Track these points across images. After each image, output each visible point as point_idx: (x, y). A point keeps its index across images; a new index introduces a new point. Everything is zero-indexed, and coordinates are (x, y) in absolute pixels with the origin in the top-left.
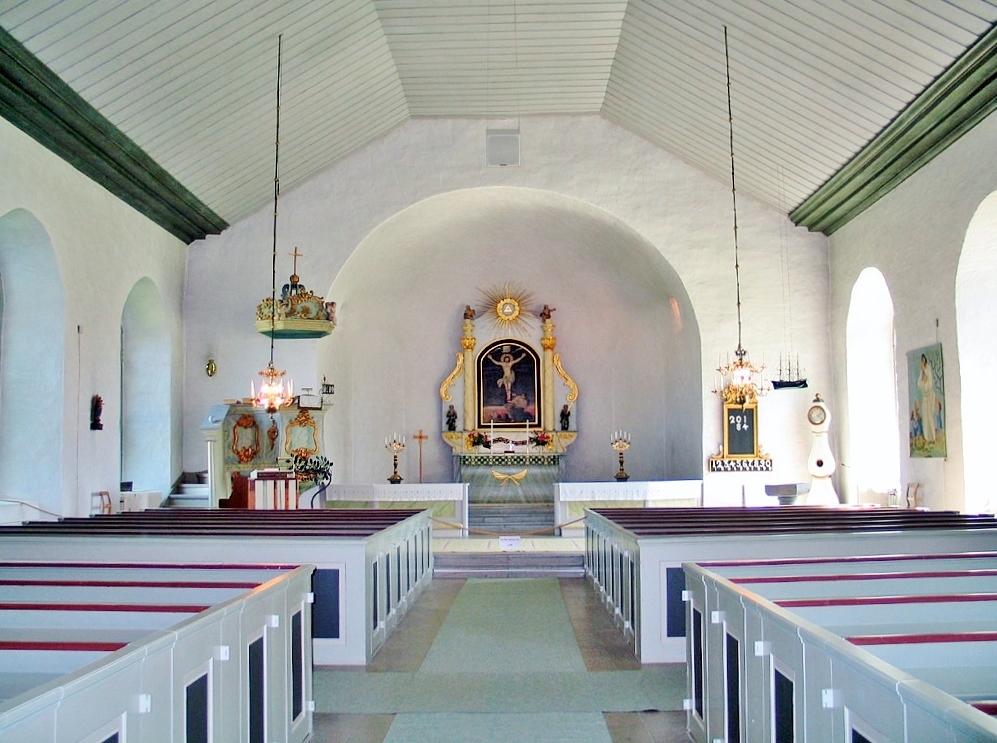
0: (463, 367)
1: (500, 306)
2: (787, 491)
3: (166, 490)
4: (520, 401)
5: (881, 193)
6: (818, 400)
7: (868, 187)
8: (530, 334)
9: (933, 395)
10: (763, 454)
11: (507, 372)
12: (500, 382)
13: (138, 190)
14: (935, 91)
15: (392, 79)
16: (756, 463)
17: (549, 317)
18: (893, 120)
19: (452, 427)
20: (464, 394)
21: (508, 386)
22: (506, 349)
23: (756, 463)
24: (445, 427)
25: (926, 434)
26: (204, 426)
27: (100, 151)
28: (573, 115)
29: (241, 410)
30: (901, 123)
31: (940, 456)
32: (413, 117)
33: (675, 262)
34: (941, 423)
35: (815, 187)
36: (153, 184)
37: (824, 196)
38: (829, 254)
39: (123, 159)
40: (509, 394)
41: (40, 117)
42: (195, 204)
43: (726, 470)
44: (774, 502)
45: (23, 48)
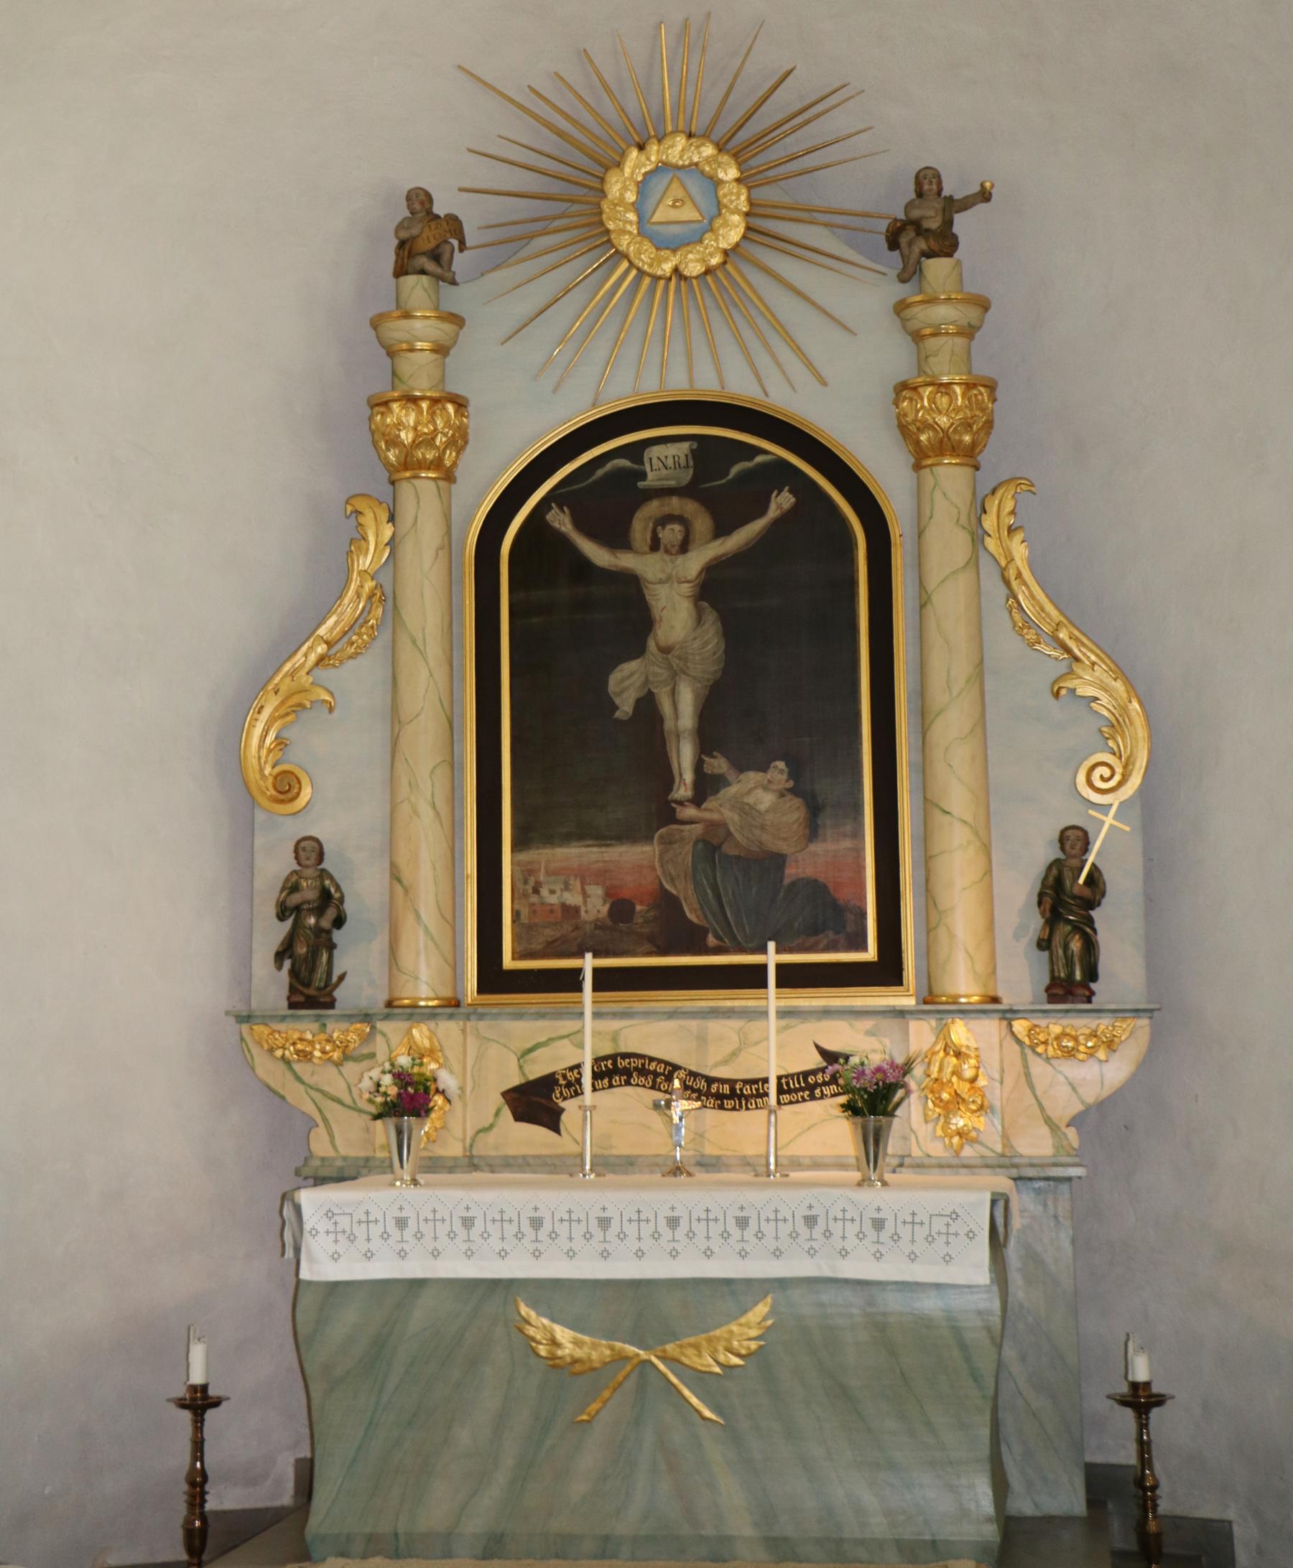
4: (758, 800)
8: (830, 366)
11: (675, 613)
12: (625, 683)
20: (398, 792)
21: (682, 710)
22: (667, 458)
40: (684, 756)
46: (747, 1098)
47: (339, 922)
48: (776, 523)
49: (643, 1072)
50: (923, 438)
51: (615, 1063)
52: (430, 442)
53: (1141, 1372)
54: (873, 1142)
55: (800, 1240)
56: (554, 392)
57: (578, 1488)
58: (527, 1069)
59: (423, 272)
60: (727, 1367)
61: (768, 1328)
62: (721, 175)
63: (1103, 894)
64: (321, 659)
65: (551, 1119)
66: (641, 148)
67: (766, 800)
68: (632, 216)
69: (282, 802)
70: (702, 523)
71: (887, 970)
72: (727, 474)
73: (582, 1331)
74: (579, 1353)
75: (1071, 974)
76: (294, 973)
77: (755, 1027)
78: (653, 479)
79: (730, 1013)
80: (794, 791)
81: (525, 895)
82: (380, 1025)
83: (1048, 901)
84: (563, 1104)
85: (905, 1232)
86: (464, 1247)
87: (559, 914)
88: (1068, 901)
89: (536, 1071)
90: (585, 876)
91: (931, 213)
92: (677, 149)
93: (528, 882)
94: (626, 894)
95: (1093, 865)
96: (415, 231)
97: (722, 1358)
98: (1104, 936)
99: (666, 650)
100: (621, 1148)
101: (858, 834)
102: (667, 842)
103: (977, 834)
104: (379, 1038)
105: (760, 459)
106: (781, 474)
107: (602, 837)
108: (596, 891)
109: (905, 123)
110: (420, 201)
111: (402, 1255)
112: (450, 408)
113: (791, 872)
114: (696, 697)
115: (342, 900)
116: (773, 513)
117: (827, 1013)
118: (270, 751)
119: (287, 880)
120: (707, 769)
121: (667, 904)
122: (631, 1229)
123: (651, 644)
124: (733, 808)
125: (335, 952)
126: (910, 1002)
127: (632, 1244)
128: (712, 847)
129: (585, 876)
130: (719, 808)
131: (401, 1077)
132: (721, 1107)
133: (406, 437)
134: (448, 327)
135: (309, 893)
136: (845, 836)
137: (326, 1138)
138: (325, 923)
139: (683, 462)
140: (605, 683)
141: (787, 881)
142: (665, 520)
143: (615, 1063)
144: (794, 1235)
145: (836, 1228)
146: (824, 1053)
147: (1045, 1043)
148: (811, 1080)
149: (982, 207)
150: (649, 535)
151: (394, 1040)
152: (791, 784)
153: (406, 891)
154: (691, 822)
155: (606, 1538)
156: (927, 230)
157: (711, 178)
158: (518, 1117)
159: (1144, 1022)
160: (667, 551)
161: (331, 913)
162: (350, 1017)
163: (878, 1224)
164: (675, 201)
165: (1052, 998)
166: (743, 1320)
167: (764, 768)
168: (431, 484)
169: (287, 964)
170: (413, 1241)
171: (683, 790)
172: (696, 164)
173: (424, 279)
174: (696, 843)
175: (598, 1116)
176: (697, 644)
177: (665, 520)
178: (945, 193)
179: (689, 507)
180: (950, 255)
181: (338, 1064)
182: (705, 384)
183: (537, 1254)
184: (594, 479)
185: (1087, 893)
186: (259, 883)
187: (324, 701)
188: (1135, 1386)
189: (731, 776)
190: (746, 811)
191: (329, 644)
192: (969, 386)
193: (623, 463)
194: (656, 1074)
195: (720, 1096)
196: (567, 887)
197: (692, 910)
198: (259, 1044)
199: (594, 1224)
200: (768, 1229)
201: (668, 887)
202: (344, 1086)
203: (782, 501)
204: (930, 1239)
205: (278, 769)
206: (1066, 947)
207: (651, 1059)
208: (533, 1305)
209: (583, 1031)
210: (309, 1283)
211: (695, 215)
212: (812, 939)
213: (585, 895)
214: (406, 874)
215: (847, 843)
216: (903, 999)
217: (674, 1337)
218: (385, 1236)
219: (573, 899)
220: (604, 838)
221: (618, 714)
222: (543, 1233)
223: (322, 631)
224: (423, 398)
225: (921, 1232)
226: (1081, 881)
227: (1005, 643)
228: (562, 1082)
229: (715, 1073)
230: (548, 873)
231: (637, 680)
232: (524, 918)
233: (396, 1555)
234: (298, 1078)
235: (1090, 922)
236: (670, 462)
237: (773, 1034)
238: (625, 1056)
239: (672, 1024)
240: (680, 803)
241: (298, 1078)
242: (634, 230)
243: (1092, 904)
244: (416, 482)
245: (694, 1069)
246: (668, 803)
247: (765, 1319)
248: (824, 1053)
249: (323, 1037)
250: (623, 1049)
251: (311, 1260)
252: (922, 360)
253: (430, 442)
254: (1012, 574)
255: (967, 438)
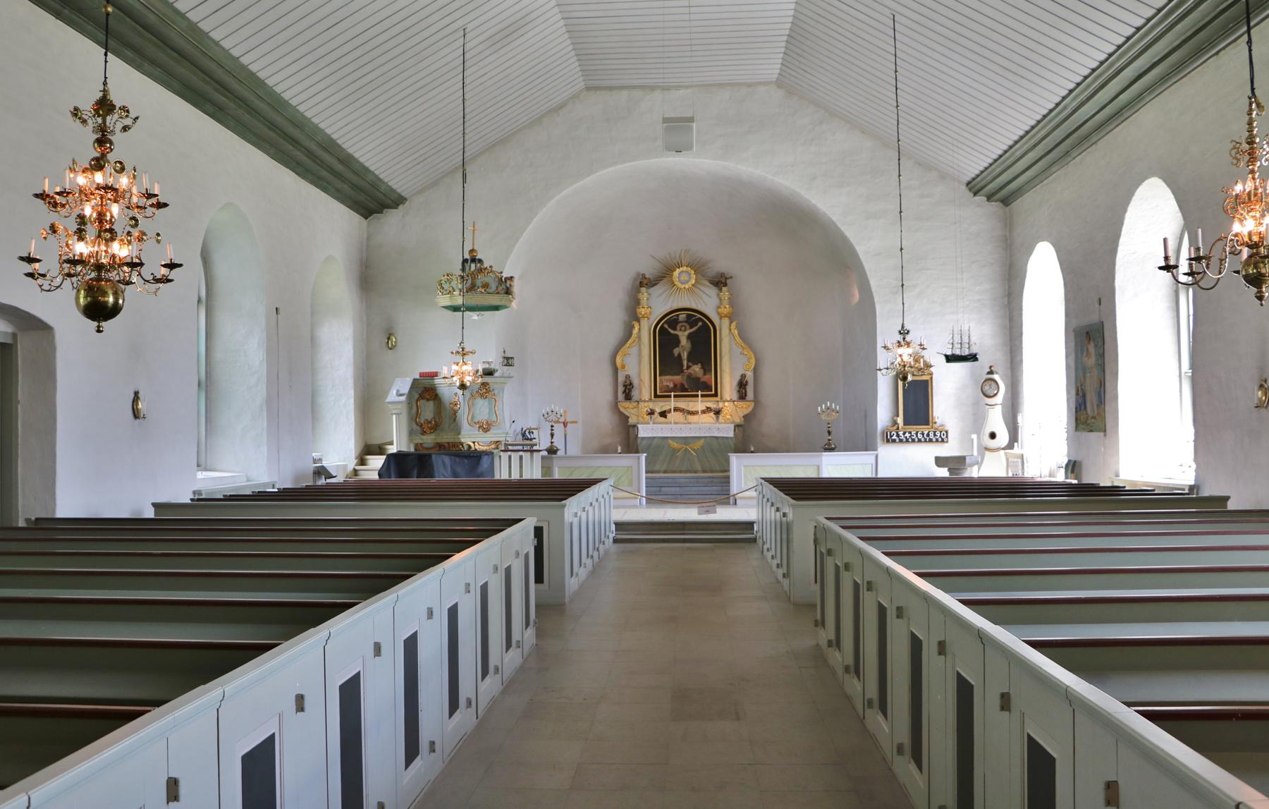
0: (639, 337)
1: (676, 273)
2: (955, 463)
3: (352, 463)
4: (697, 369)
5: (1053, 169)
6: (991, 372)
7: (1040, 164)
8: (708, 302)
9: (1096, 372)
10: (939, 421)
11: (684, 341)
12: (676, 351)
13: (324, 173)
14: (1093, 82)
15: (564, 45)
16: (931, 435)
17: (725, 285)
18: (1057, 105)
19: (628, 397)
20: (640, 363)
21: (685, 356)
22: (682, 317)
23: (931, 435)
24: (621, 396)
25: (1092, 405)
26: (389, 399)
27: (295, 142)
28: (749, 85)
29: (427, 382)
30: (1065, 108)
31: (1099, 431)
32: (588, 89)
33: (850, 233)
34: (1101, 401)
35: (990, 161)
36: (339, 167)
37: (999, 170)
38: (1008, 224)
39: (313, 147)
40: (685, 363)
41: (247, 118)
42: (376, 183)
43: (901, 441)
44: (943, 473)
45: (187, 19)
71: (716, 395)
88: (742, 385)
93: (661, 382)
109: (721, 264)
121: (682, 385)
128: (689, 376)
175: (672, 416)
209: (672, 403)
237: (699, 404)
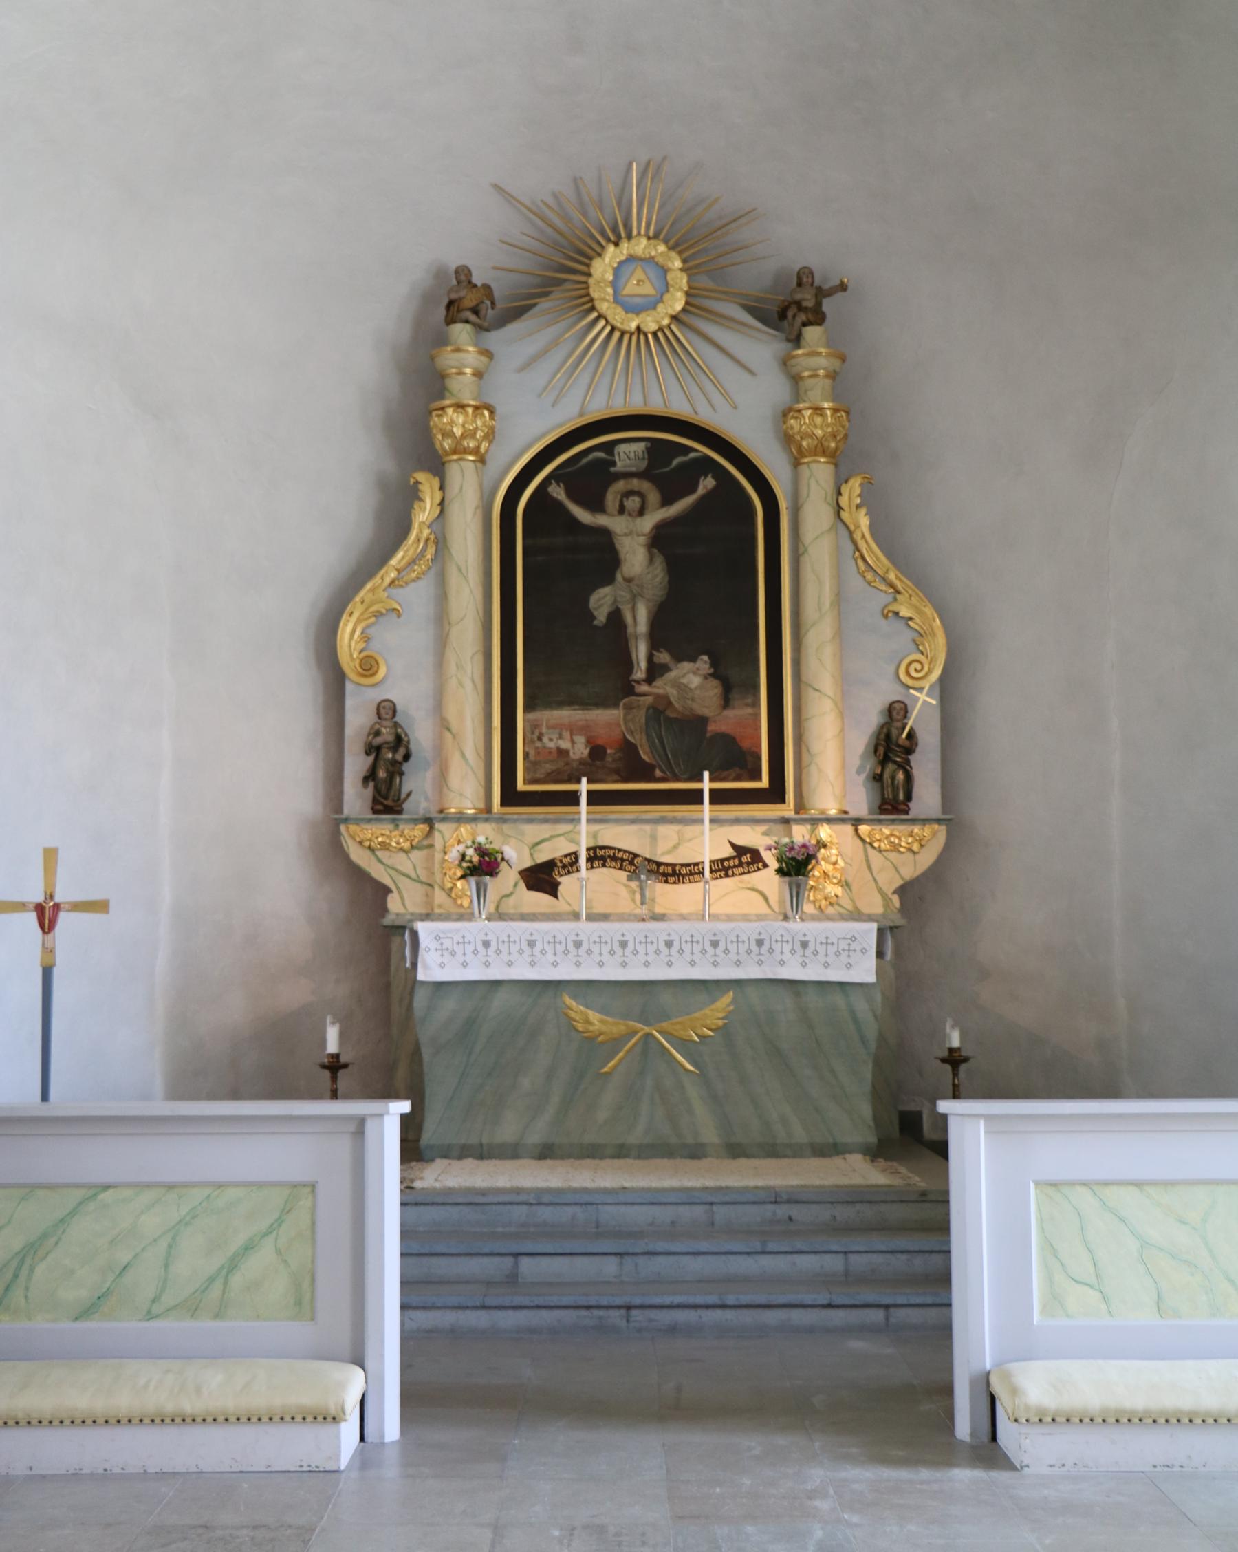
4: (691, 680)
8: (738, 393)
11: (635, 556)
12: (601, 601)
21: (639, 620)
22: (630, 452)
40: (641, 652)
46: (683, 876)
47: (407, 757)
48: (703, 497)
49: (614, 858)
50: (804, 443)
51: (595, 853)
52: (472, 434)
53: (955, 1040)
54: (797, 895)
55: (753, 955)
56: (553, 406)
57: (602, 1115)
58: (535, 856)
59: (467, 321)
60: (703, 1037)
61: (730, 1012)
62: (670, 265)
63: (917, 745)
64: (392, 582)
65: (552, 889)
66: (616, 244)
67: (695, 681)
68: (610, 290)
69: (365, 676)
70: (653, 496)
71: (776, 793)
72: (670, 463)
73: (607, 1014)
74: (604, 1028)
75: (896, 796)
76: (377, 790)
77: (690, 830)
78: (621, 465)
79: (674, 821)
80: (714, 675)
81: (532, 742)
82: (437, 825)
83: (881, 750)
84: (560, 879)
85: (821, 949)
86: (529, 959)
87: (555, 754)
88: (891, 750)
89: (542, 857)
90: (573, 729)
91: (808, 297)
92: (641, 246)
94: (600, 742)
95: (912, 729)
96: (462, 294)
97: (699, 1032)
98: (917, 772)
99: (629, 580)
100: (599, 909)
101: (756, 704)
102: (628, 708)
103: (836, 704)
104: (437, 834)
105: (692, 455)
106: (707, 465)
107: (585, 704)
108: (580, 740)
110: (463, 274)
111: (487, 964)
112: (486, 413)
113: (712, 728)
114: (649, 612)
115: (408, 742)
116: (701, 491)
117: (737, 821)
118: (357, 643)
119: (372, 728)
120: (656, 660)
121: (628, 749)
122: (641, 949)
123: (619, 577)
124: (673, 686)
125: (404, 778)
126: (790, 813)
127: (642, 957)
128: (659, 713)
129: (573, 729)
130: (663, 686)
131: (481, 851)
132: (666, 882)
133: (458, 432)
134: (484, 359)
135: (387, 735)
136: (747, 705)
137: (399, 901)
138: (399, 757)
139: (641, 455)
140: (587, 601)
141: (708, 735)
142: (628, 494)
143: (595, 853)
144: (749, 952)
145: (777, 947)
146: (734, 846)
147: (879, 841)
148: (726, 864)
149: (840, 294)
150: (617, 504)
151: (447, 836)
152: (711, 671)
153: (454, 737)
154: (644, 695)
155: (622, 1146)
156: (806, 308)
157: (662, 267)
158: (530, 888)
159: (943, 828)
160: (630, 515)
161: (402, 751)
162: (415, 821)
163: (804, 945)
164: (639, 281)
165: (882, 810)
166: (713, 1007)
167: (693, 659)
168: (471, 465)
169: (371, 784)
170: (494, 956)
171: (640, 673)
172: (653, 258)
173: (468, 326)
174: (648, 709)
176: (650, 576)
177: (628, 494)
178: (816, 284)
179: (645, 486)
180: (819, 324)
181: (406, 852)
182: (656, 405)
183: (578, 964)
184: (579, 466)
185: (907, 743)
186: (349, 731)
187: (394, 609)
188: (951, 1050)
189: (671, 664)
190: (682, 688)
191: (398, 571)
192: (835, 410)
193: (601, 455)
194: (622, 860)
195: (665, 875)
196: (561, 737)
197: (645, 753)
198: (353, 838)
199: (616, 945)
200: (733, 948)
201: (628, 737)
202: (411, 866)
203: (707, 483)
204: (838, 954)
205: (364, 654)
206: (893, 778)
207: (620, 850)
208: (574, 997)
209: (582, 830)
210: (423, 983)
211: (653, 292)
212: (725, 774)
213: (573, 742)
214: (454, 725)
215: (749, 710)
216: (787, 809)
217: (667, 1017)
218: (475, 952)
219: (565, 744)
220: (587, 704)
221: (596, 622)
222: (582, 951)
223: (393, 562)
224: (469, 406)
225: (832, 949)
226: (904, 736)
227: (855, 583)
228: (559, 865)
229: (662, 860)
230: (548, 727)
231: (609, 600)
232: (532, 757)
233: (481, 1157)
234: (380, 861)
235: (908, 762)
236: (632, 455)
237: (704, 836)
238: (602, 848)
239: (634, 827)
240: (638, 682)
241: (380, 861)
242: (611, 298)
243: (909, 751)
244: (462, 463)
245: (648, 856)
246: (629, 682)
247: (728, 1005)
248: (734, 846)
249: (396, 833)
250: (601, 844)
251: (426, 967)
252: (797, 395)
253: (472, 434)
254: (858, 536)
255: (833, 445)
